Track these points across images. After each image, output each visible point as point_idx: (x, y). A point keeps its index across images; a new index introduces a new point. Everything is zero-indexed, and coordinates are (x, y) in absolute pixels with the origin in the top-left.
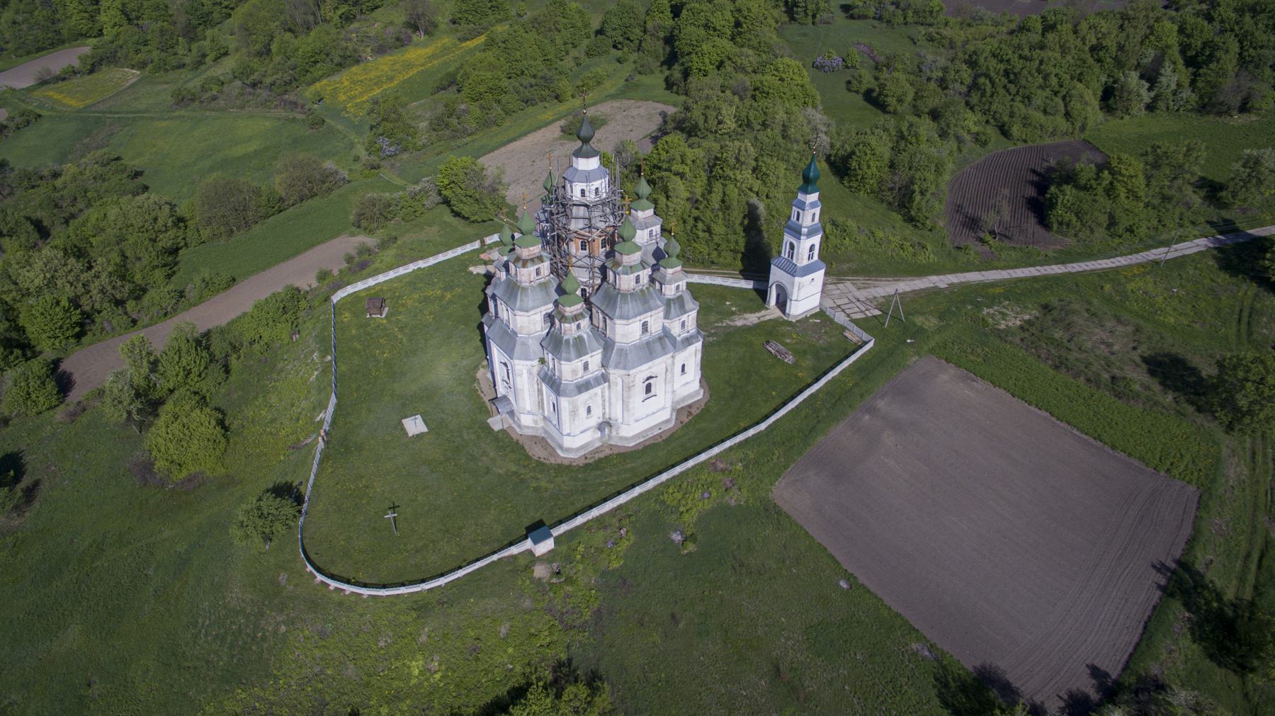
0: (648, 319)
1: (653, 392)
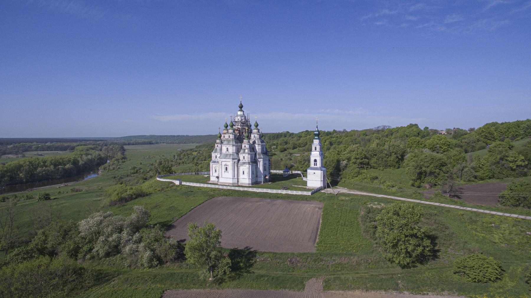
0: (228, 147)
1: (227, 171)
